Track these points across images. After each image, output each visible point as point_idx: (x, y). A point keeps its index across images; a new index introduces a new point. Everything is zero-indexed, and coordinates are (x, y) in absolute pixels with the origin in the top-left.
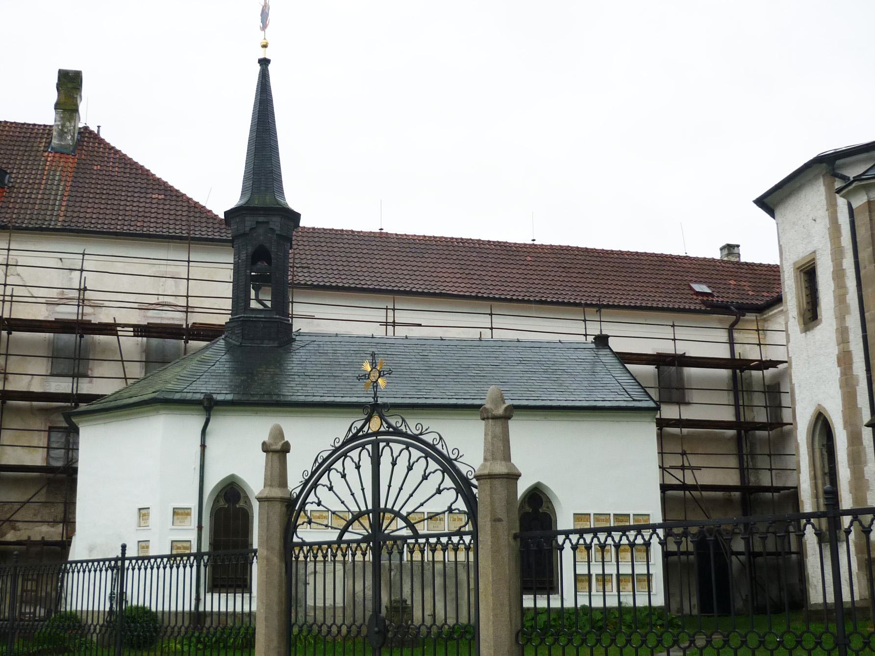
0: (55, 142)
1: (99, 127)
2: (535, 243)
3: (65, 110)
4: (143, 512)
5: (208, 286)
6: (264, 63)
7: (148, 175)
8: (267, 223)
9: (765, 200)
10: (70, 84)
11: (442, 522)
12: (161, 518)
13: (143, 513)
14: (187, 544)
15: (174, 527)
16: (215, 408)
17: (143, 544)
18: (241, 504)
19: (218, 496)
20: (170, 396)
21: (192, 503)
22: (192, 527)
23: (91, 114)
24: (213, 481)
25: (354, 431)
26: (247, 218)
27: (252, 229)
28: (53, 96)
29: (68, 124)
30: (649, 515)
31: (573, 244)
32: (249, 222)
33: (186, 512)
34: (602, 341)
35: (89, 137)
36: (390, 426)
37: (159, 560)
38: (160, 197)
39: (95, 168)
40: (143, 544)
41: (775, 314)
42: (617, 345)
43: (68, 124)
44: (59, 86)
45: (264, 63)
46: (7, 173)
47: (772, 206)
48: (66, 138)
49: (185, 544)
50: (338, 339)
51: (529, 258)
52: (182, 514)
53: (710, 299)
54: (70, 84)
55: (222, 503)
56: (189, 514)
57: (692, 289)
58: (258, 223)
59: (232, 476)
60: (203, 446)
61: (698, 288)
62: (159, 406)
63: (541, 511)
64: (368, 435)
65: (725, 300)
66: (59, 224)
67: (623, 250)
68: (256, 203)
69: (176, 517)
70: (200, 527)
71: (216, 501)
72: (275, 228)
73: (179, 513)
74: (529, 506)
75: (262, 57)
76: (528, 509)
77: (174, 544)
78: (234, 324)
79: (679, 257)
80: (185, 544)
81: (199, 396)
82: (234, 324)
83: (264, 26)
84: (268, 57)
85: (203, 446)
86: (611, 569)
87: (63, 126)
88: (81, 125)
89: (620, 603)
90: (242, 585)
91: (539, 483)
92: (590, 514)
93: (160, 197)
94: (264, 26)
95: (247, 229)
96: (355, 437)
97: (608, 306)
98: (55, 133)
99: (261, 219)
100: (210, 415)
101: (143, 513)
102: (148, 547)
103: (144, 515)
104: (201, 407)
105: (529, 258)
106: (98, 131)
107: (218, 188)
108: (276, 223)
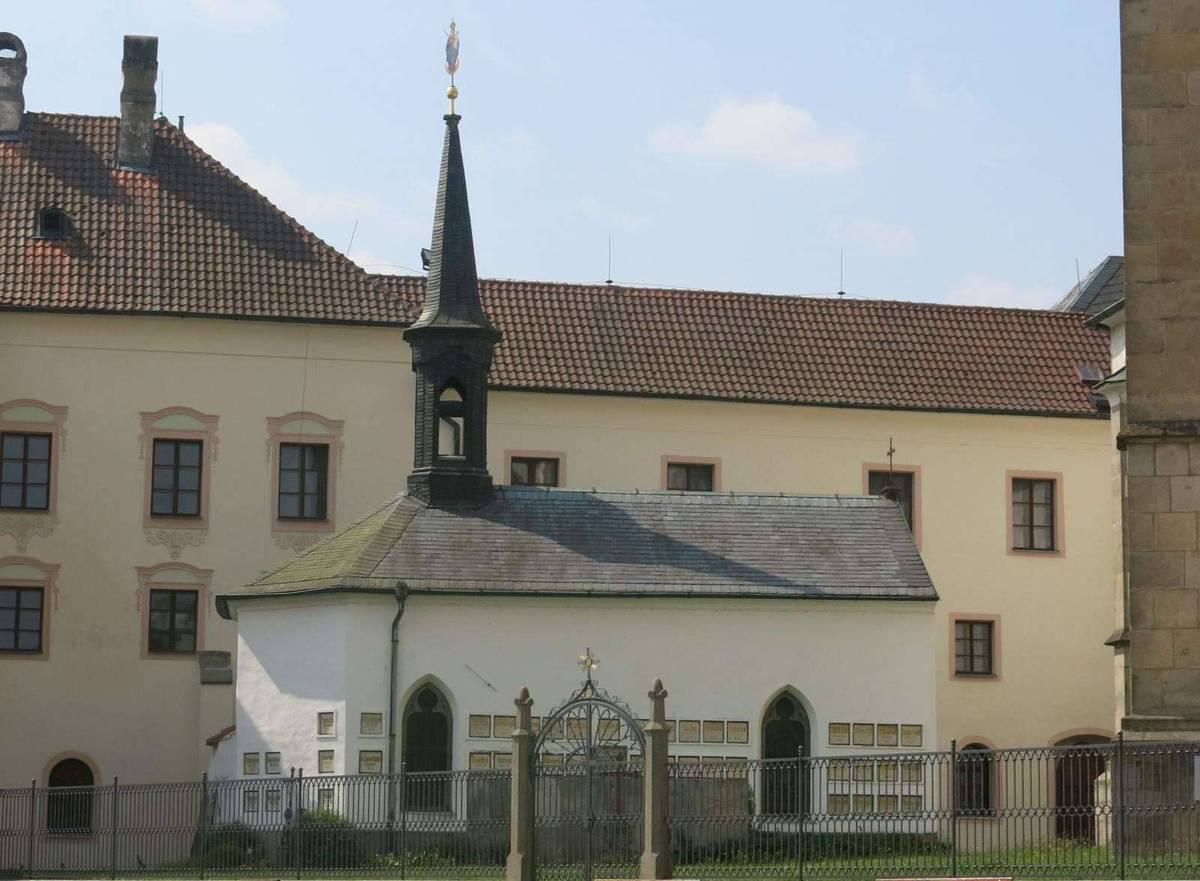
1: (181, 118)
2: (844, 297)
4: (324, 716)
5: (370, 402)
6: (452, 121)
7: (264, 207)
10: (140, 56)
17: (251, 757)
18: (438, 709)
21: (382, 707)
22: (383, 736)
23: (169, 104)
24: (408, 681)
25: (575, 696)
29: (142, 125)
31: (902, 299)
36: (597, 695)
37: (314, 780)
40: (251, 757)
45: (452, 121)
48: (139, 146)
54: (140, 56)
55: (417, 709)
60: (395, 641)
64: (584, 700)
70: (392, 736)
71: (410, 705)
73: (369, 720)
81: (386, 584)
83: (452, 68)
85: (395, 641)
86: (898, 792)
91: (788, 686)
94: (452, 68)
96: (576, 700)
99: (452, 342)
103: (326, 720)
104: (392, 596)
106: (181, 124)
107: (389, 240)
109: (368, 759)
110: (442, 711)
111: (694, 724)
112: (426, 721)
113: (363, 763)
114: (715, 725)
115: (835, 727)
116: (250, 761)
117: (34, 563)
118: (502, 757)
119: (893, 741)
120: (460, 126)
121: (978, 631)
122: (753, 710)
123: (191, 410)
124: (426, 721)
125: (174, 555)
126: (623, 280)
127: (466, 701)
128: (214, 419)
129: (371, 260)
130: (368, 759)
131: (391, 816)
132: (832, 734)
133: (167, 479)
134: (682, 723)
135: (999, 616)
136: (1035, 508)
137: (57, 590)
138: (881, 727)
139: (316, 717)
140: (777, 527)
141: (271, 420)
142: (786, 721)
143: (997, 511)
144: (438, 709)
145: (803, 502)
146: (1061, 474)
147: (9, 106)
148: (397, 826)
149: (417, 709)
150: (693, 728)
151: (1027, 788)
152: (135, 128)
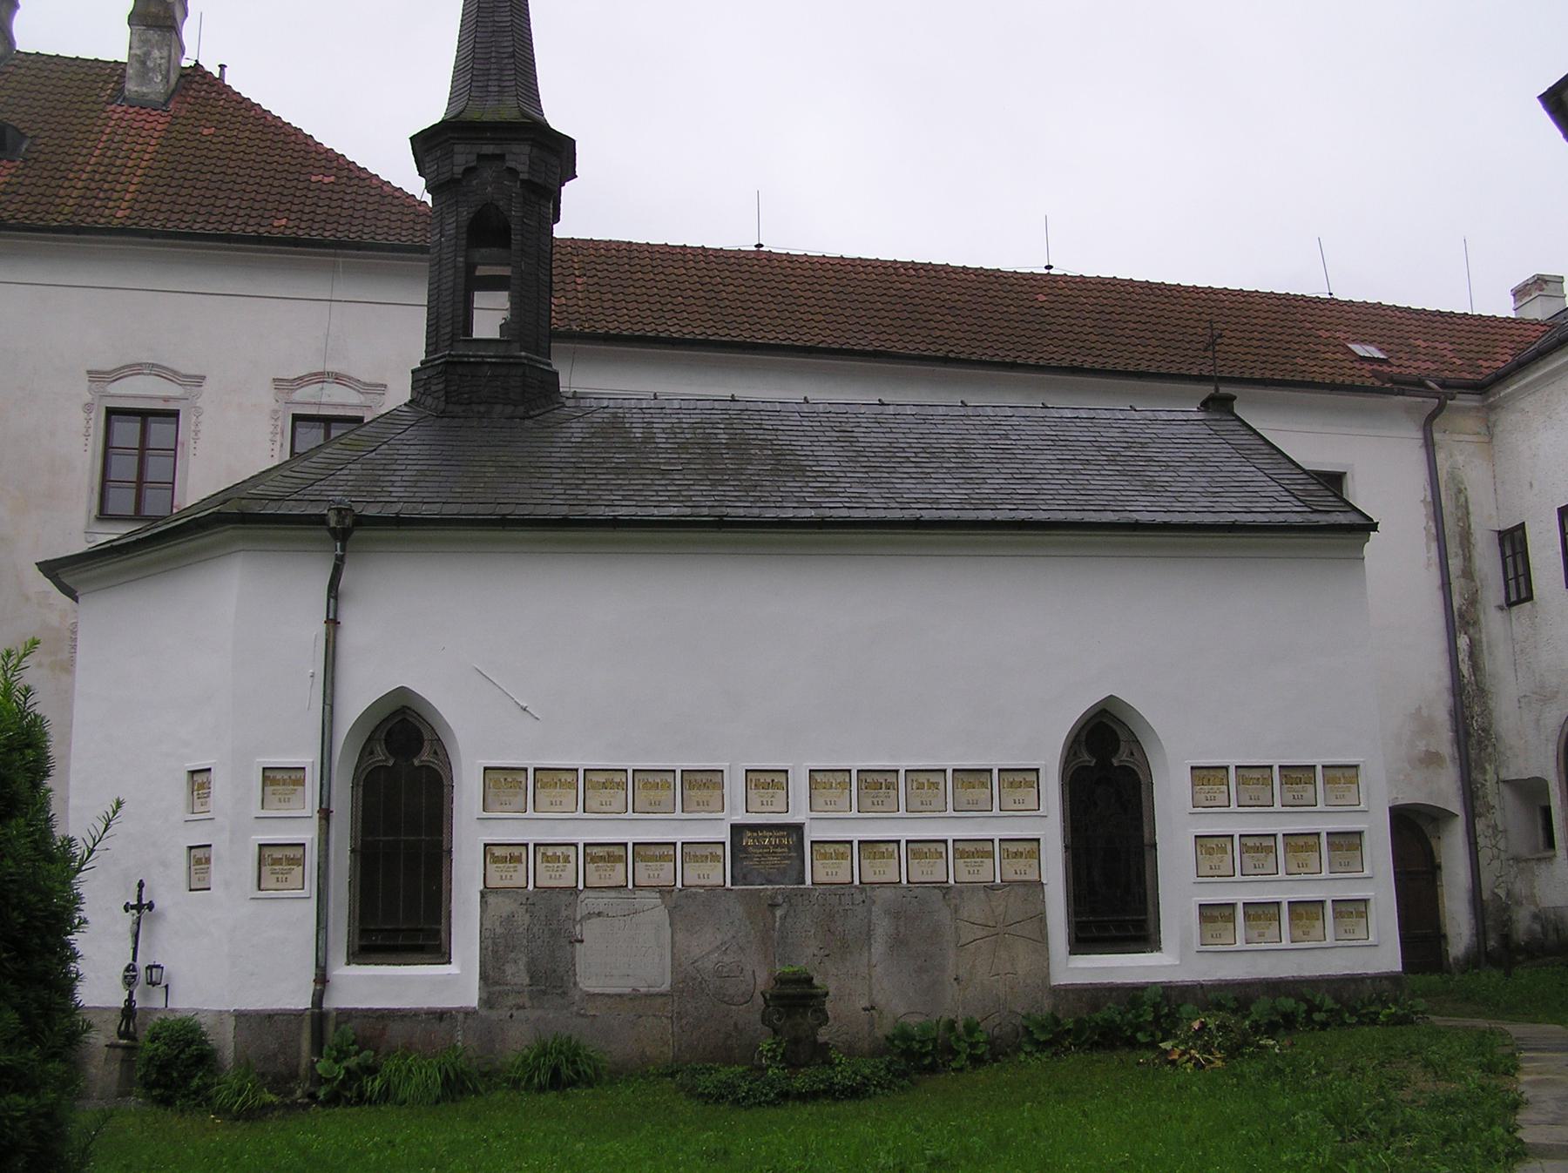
0: (131, 87)
1: (222, 67)
2: (1052, 271)
8: (501, 157)
10: (222, 67)
11: (893, 793)
12: (235, 791)
13: (199, 778)
14: (298, 852)
15: (486, 815)
17: (199, 853)
18: (425, 756)
19: (369, 739)
20: (256, 508)
21: (307, 757)
23: (205, 41)
24: (357, 700)
26: (457, 148)
27: (469, 171)
30: (1356, 767)
32: (463, 156)
33: (295, 775)
35: (202, 87)
38: (326, 180)
39: (206, 132)
41: (1512, 394)
46: (24, 136)
49: (290, 852)
51: (1041, 298)
55: (380, 755)
56: (301, 782)
58: (481, 157)
59: (402, 691)
60: (333, 623)
61: (1361, 350)
62: (229, 532)
63: (1115, 762)
65: (1415, 372)
68: (474, 115)
69: (269, 789)
70: (325, 814)
71: (367, 750)
72: (520, 168)
74: (1091, 752)
76: (1087, 758)
77: (267, 852)
78: (430, 372)
80: (516, 851)
82: (430, 372)
85: (333, 623)
89: (318, 998)
91: (1111, 698)
92: (1226, 768)
93: (326, 180)
95: (458, 170)
99: (489, 149)
101: (199, 778)
102: (208, 860)
105: (1041, 298)
107: (373, 100)
108: (520, 156)
109: (277, 861)
111: (934, 778)
112: (396, 783)
113: (266, 869)
114: (972, 778)
115: (1203, 774)
116: (199, 861)
118: (550, 851)
119: (1266, 800)
122: (1047, 754)
124: (396, 783)
126: (777, 243)
127: (473, 747)
128: (199, 380)
129: (208, 69)
130: (277, 861)
131: (322, 979)
132: (491, 867)
134: (910, 775)
138: (1336, 840)
139: (185, 776)
142: (1105, 769)
148: (338, 1000)
150: (935, 785)
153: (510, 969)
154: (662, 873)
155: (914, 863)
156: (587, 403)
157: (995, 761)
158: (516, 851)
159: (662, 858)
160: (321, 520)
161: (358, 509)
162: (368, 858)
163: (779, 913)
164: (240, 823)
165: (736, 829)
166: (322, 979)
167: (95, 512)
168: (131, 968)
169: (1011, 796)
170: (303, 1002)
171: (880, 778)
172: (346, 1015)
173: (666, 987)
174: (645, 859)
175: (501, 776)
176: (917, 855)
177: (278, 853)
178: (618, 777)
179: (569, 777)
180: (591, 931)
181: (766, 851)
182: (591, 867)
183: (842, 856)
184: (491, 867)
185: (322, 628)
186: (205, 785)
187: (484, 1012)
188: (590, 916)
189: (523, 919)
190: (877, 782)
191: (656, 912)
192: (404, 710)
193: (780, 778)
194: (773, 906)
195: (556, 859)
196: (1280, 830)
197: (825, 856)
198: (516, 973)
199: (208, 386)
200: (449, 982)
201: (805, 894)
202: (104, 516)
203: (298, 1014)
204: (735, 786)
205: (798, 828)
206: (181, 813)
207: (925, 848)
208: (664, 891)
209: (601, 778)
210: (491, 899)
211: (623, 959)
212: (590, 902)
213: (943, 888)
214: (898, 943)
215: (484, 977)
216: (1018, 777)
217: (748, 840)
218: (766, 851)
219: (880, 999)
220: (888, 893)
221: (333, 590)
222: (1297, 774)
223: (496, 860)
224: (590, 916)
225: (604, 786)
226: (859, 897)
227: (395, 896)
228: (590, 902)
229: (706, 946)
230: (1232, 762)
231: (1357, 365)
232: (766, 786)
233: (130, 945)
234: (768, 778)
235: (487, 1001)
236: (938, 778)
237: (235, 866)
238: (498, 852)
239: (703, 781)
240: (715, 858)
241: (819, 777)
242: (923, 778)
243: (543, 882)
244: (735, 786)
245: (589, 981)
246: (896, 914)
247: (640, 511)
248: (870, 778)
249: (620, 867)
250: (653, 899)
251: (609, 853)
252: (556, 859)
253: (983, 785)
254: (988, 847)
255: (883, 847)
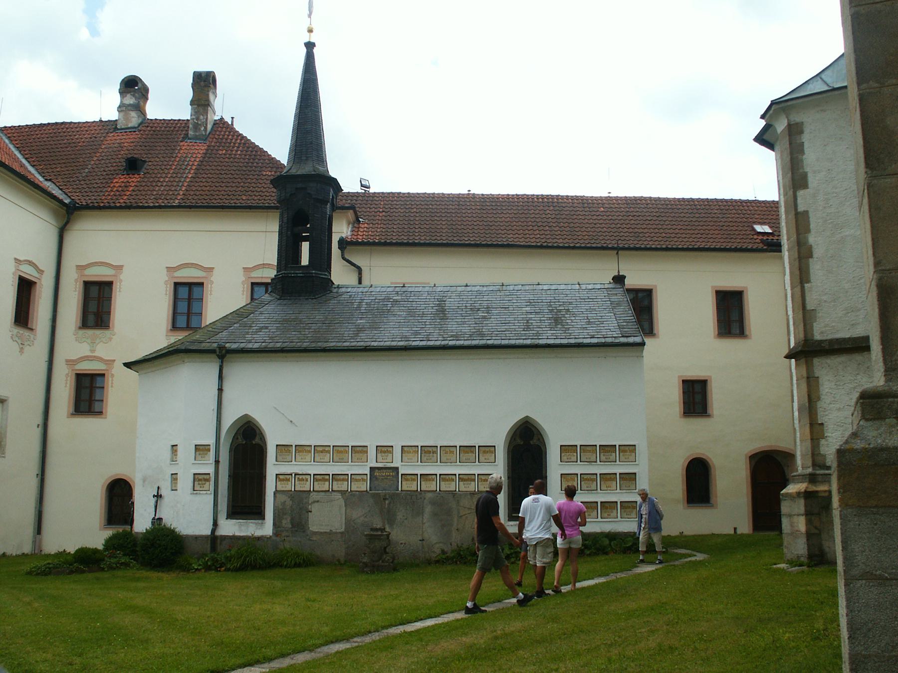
0: (191, 133)
2: (611, 195)
3: (199, 105)
6: (310, 46)
9: (765, 137)
10: (204, 83)
12: (186, 453)
16: (228, 355)
18: (257, 440)
21: (211, 441)
23: (223, 106)
24: (228, 420)
28: (188, 93)
29: (201, 117)
34: (619, 280)
42: (629, 282)
43: (201, 117)
44: (194, 85)
45: (310, 46)
47: (772, 142)
49: (205, 477)
50: (469, 289)
52: (203, 450)
53: (771, 237)
56: (209, 450)
57: (754, 230)
58: (297, 189)
59: (246, 415)
60: (220, 390)
61: (759, 228)
63: (531, 442)
66: (177, 201)
67: (693, 197)
70: (217, 462)
71: (235, 438)
73: (201, 449)
75: (307, 40)
79: (747, 201)
80: (205, 477)
84: (312, 41)
85: (220, 390)
87: (198, 119)
88: (217, 118)
89: (213, 531)
90: (257, 513)
94: (310, 16)
97: (624, 249)
98: (191, 126)
99: (300, 185)
100: (222, 362)
104: (214, 356)
109: (200, 480)
110: (260, 442)
111: (452, 449)
112: (246, 448)
113: (196, 483)
114: (467, 449)
115: (565, 449)
117: (100, 359)
118: (301, 477)
120: (315, 50)
121: (698, 388)
123: (193, 264)
124: (246, 448)
125: (93, 351)
128: (211, 269)
130: (200, 480)
131: (215, 524)
133: (195, 305)
135: (656, 286)
136: (730, 312)
137: (113, 375)
139: (170, 447)
140: (530, 303)
141: (246, 269)
143: (707, 312)
144: (257, 440)
145: (553, 287)
146: (746, 288)
147: (133, 114)
149: (241, 440)
150: (453, 452)
151: (732, 485)
152: (198, 119)
153: (284, 522)
154: (344, 486)
155: (442, 483)
156: (343, 290)
157: (476, 442)
158: (288, 477)
159: (343, 480)
160: (212, 351)
161: (227, 345)
162: (234, 477)
163: (387, 502)
164: (188, 466)
165: (397, 468)
166: (215, 524)
167: (170, 327)
168: (154, 519)
169: (464, 456)
170: (208, 532)
171: (430, 449)
172: (224, 538)
173: (343, 530)
174: (337, 480)
175: (283, 448)
176: (444, 480)
177: (201, 477)
178: (327, 449)
179: (308, 448)
180: (314, 508)
181: (383, 476)
182: (316, 483)
183: (414, 480)
184: (278, 483)
185: (224, 388)
186: (176, 451)
187: (274, 538)
188: (314, 502)
189: (289, 503)
190: (428, 452)
191: (339, 500)
192: (249, 422)
193: (390, 449)
194: (385, 499)
195: (302, 480)
196: (598, 472)
197: (407, 480)
198: (286, 523)
199: (215, 272)
200: (266, 528)
201: (398, 495)
202: (174, 327)
203: (206, 537)
204: (372, 452)
205: (397, 468)
206: (168, 461)
207: (447, 477)
208: (343, 493)
209: (321, 449)
210: (277, 495)
211: (327, 518)
212: (314, 496)
213: (453, 493)
214: (435, 514)
215: (274, 524)
216: (487, 449)
217: (377, 473)
218: (383, 476)
219: (426, 536)
220: (429, 495)
221: (221, 377)
222: (607, 449)
223: (281, 480)
224: (314, 502)
225: (322, 452)
226: (419, 496)
227: (245, 496)
228: (314, 496)
229: (358, 514)
230: (578, 443)
231: (755, 237)
232: (385, 452)
233: (154, 509)
234: (385, 449)
235: (276, 533)
236: (454, 449)
237: (185, 482)
238: (281, 477)
239: (360, 451)
240: (363, 480)
241: (405, 449)
242: (447, 449)
243: (405, 488)
244: (372, 452)
245: (313, 527)
246: (433, 503)
247: (339, 344)
248: (426, 449)
249: (327, 483)
250: (339, 496)
251: (323, 478)
252: (302, 480)
253: (472, 452)
254: (473, 477)
255: (430, 477)
